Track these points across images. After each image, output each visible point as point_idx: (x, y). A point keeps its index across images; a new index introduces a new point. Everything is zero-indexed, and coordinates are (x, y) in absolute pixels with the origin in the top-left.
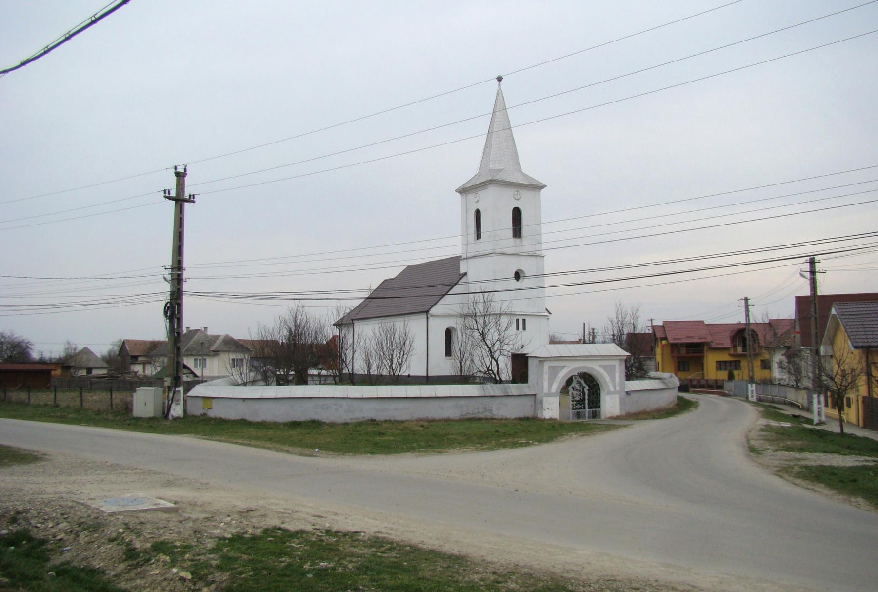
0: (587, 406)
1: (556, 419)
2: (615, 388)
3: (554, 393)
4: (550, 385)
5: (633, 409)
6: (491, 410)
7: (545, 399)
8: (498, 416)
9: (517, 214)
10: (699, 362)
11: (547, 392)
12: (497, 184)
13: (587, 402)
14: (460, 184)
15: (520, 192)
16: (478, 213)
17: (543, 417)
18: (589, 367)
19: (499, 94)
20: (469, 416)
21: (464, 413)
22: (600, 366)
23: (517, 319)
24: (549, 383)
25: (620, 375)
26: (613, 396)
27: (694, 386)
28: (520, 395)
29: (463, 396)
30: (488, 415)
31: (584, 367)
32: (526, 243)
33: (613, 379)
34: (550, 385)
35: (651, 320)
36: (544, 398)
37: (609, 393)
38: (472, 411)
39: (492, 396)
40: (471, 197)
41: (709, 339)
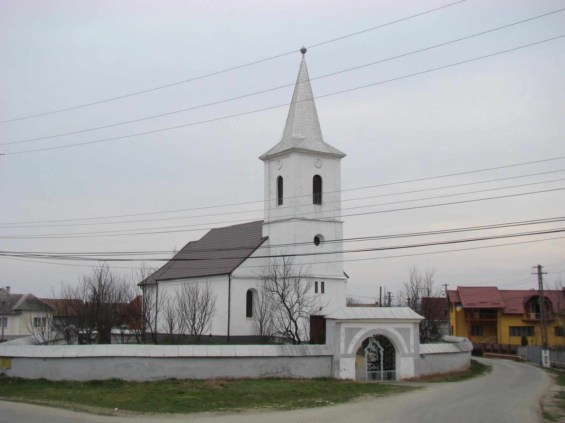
1: (352, 380)
2: (409, 351)
3: (350, 354)
4: (347, 347)
5: (427, 372)
6: (289, 370)
7: (342, 360)
8: (296, 375)
9: (317, 181)
10: (493, 328)
12: (301, 152)
13: (382, 363)
15: (321, 161)
16: (280, 179)
17: (340, 378)
18: (384, 329)
19: (303, 65)
21: (263, 373)
23: (322, 282)
24: (345, 344)
25: (415, 339)
26: (408, 358)
28: (318, 356)
30: (286, 374)
31: (379, 329)
32: (325, 211)
34: (347, 347)
35: (446, 285)
36: (340, 358)
37: (404, 355)
38: (271, 371)
39: (291, 357)
40: (274, 164)
41: (502, 305)
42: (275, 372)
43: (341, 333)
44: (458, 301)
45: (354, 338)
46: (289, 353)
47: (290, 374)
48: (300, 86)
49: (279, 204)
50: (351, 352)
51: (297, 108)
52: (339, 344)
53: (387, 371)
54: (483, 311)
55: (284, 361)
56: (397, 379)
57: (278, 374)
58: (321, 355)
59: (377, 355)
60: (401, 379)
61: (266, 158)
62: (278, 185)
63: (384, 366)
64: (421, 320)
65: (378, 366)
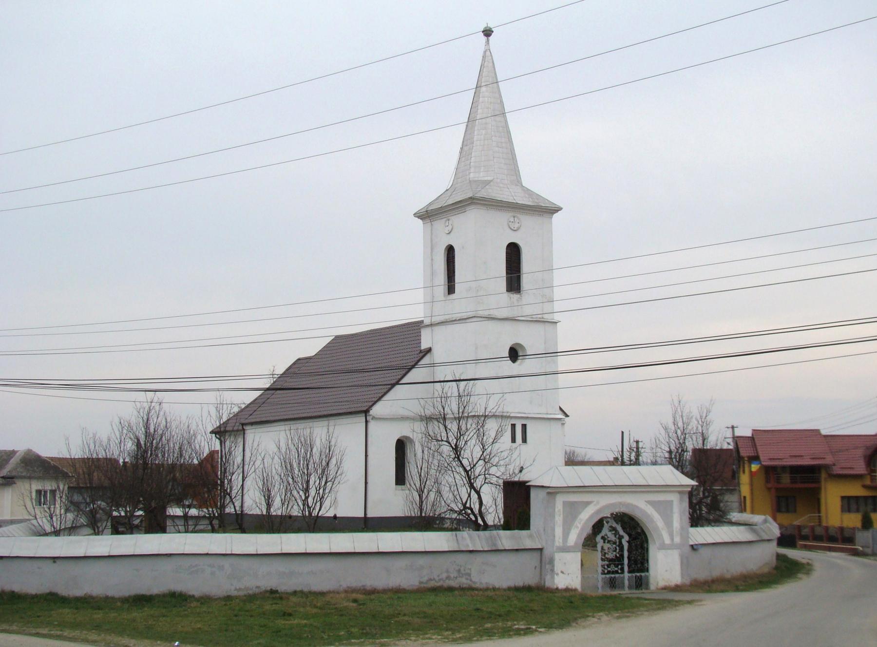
0: (626, 568)
1: (576, 590)
2: (672, 540)
6: (469, 575)
7: (558, 556)
9: (513, 253)
10: (813, 499)
11: (561, 545)
13: (626, 561)
14: (421, 204)
15: (519, 219)
16: (450, 251)
17: (555, 587)
20: (432, 584)
21: (425, 579)
22: (646, 501)
23: (522, 425)
25: (681, 519)
26: (669, 551)
27: (805, 538)
28: (517, 550)
29: (400, 550)
30: (464, 581)
31: (620, 503)
33: (669, 524)
35: (733, 427)
36: (556, 554)
37: (663, 547)
38: (438, 576)
40: (440, 225)
41: (829, 460)
42: (444, 579)
43: (556, 510)
44: (753, 454)
45: (578, 518)
46: (468, 546)
47: (471, 580)
48: (483, 92)
49: (449, 293)
50: (574, 542)
51: (478, 129)
52: (553, 530)
53: (634, 575)
54: (796, 470)
55: (461, 559)
56: (652, 587)
57: (451, 581)
58: (523, 548)
59: (618, 548)
60: (659, 587)
61: (427, 215)
62: (447, 260)
63: (629, 566)
64: (691, 487)
65: (620, 567)
